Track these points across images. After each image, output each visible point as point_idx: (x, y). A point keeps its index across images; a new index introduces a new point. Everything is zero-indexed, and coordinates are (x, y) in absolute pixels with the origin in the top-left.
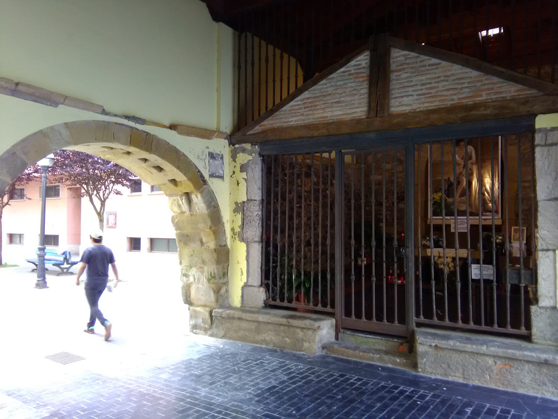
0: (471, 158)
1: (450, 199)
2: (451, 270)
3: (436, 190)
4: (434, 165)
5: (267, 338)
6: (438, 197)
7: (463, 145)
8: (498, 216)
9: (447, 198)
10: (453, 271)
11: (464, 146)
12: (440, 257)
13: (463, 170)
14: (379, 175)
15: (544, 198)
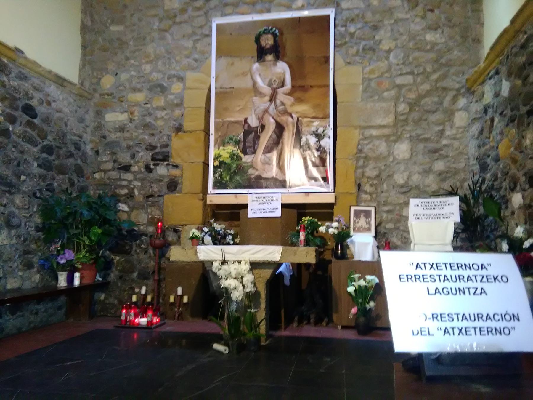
0: (283, 85)
1: (247, 156)
2: (248, 290)
3: (222, 143)
4: (221, 95)
5: (13, 181)
6: (227, 153)
7: (270, 61)
8: (329, 187)
9: (242, 155)
10: (250, 292)
11: (272, 62)
12: (224, 262)
13: (270, 105)
14: (122, 113)
15: (166, 170)
